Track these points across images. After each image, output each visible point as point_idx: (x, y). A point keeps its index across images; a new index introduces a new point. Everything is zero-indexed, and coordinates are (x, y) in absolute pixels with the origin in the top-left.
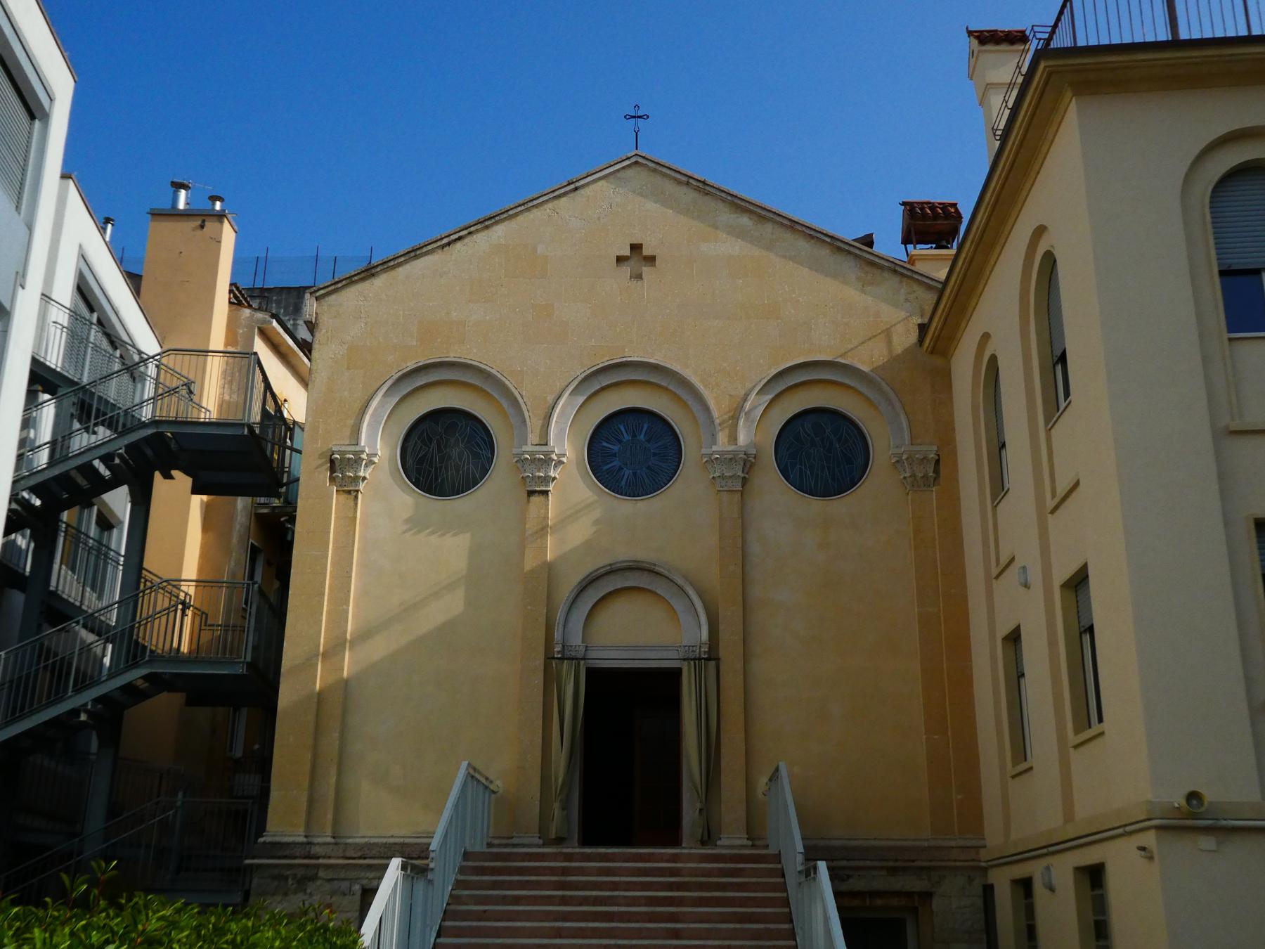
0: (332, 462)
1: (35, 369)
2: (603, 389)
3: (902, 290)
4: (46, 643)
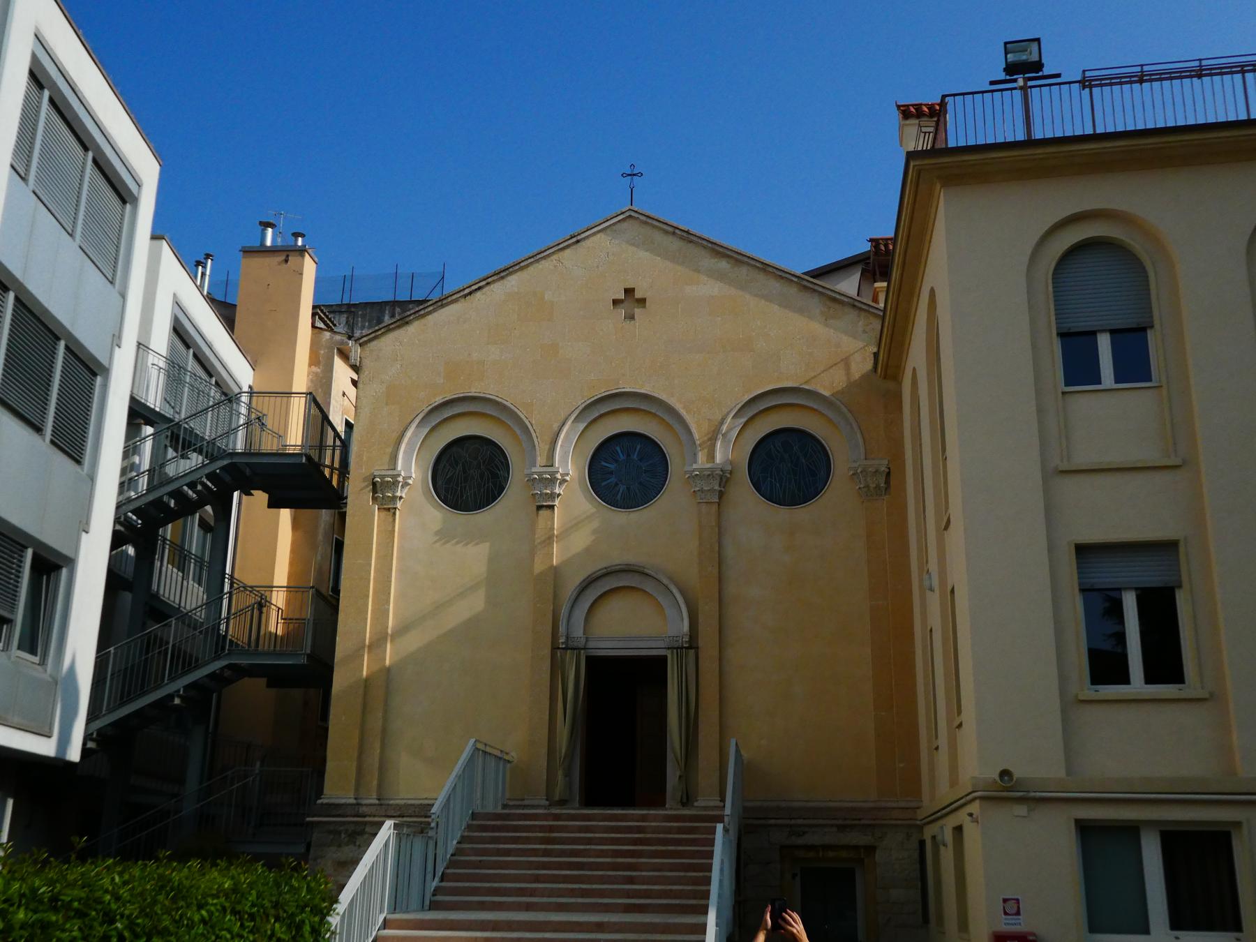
0: (374, 484)
1: (133, 406)
2: (601, 416)
3: (860, 323)
4: (159, 634)
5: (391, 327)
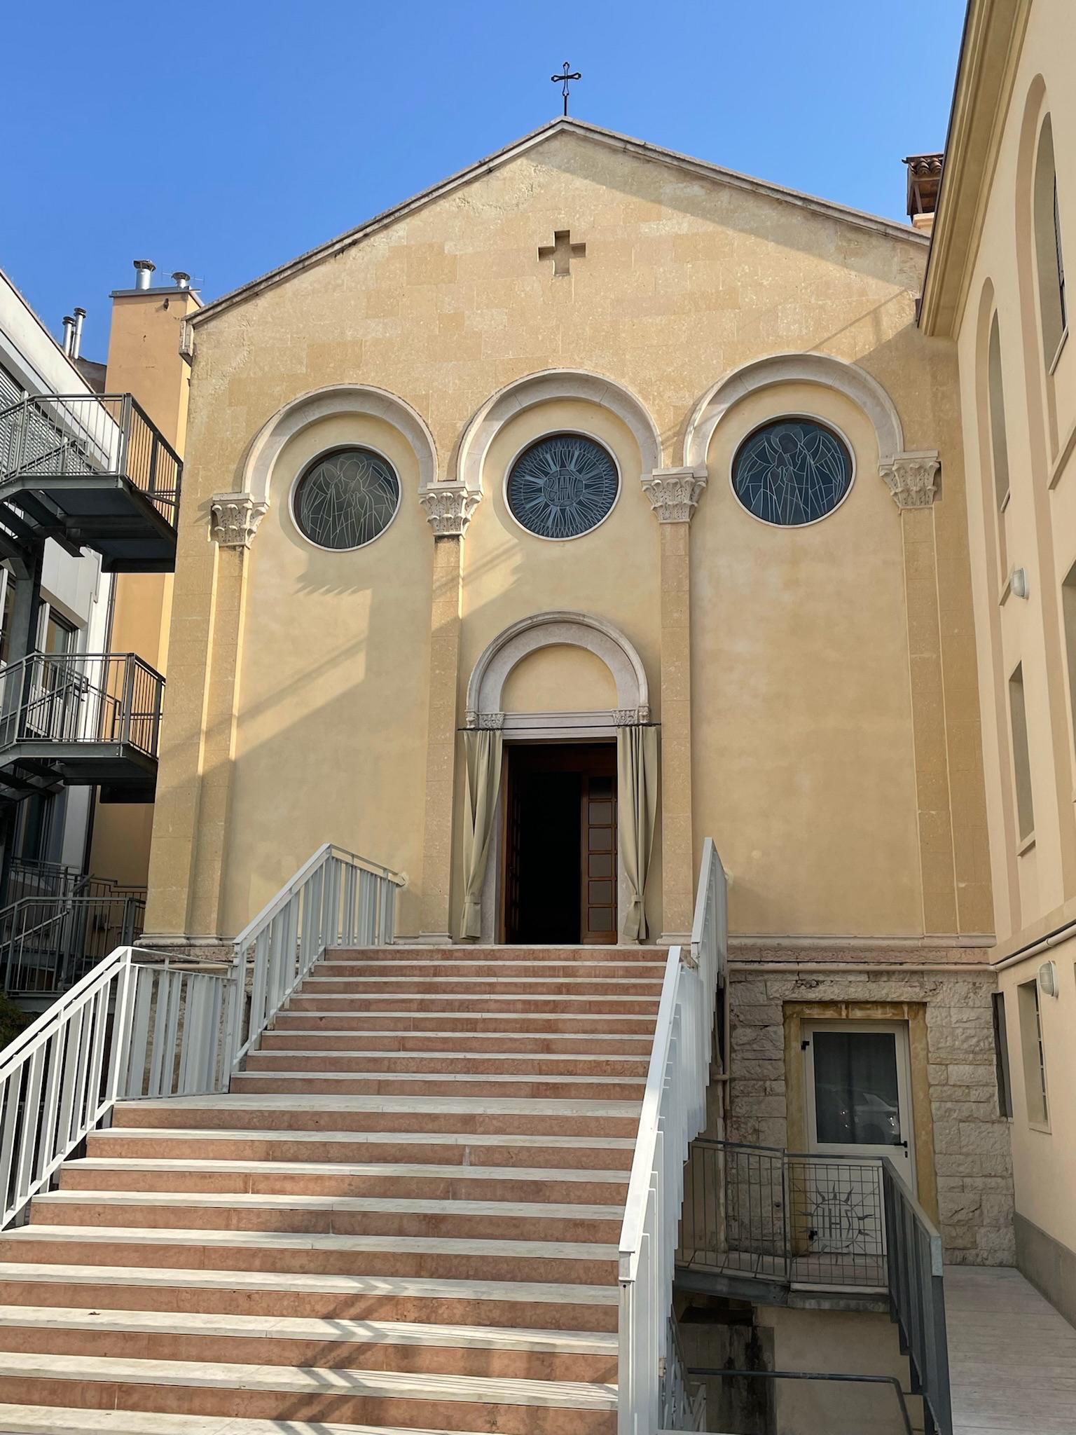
0: (214, 514)
3: (896, 259)
5: (234, 301)
